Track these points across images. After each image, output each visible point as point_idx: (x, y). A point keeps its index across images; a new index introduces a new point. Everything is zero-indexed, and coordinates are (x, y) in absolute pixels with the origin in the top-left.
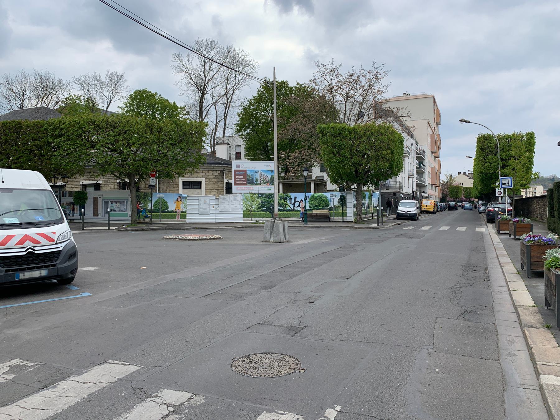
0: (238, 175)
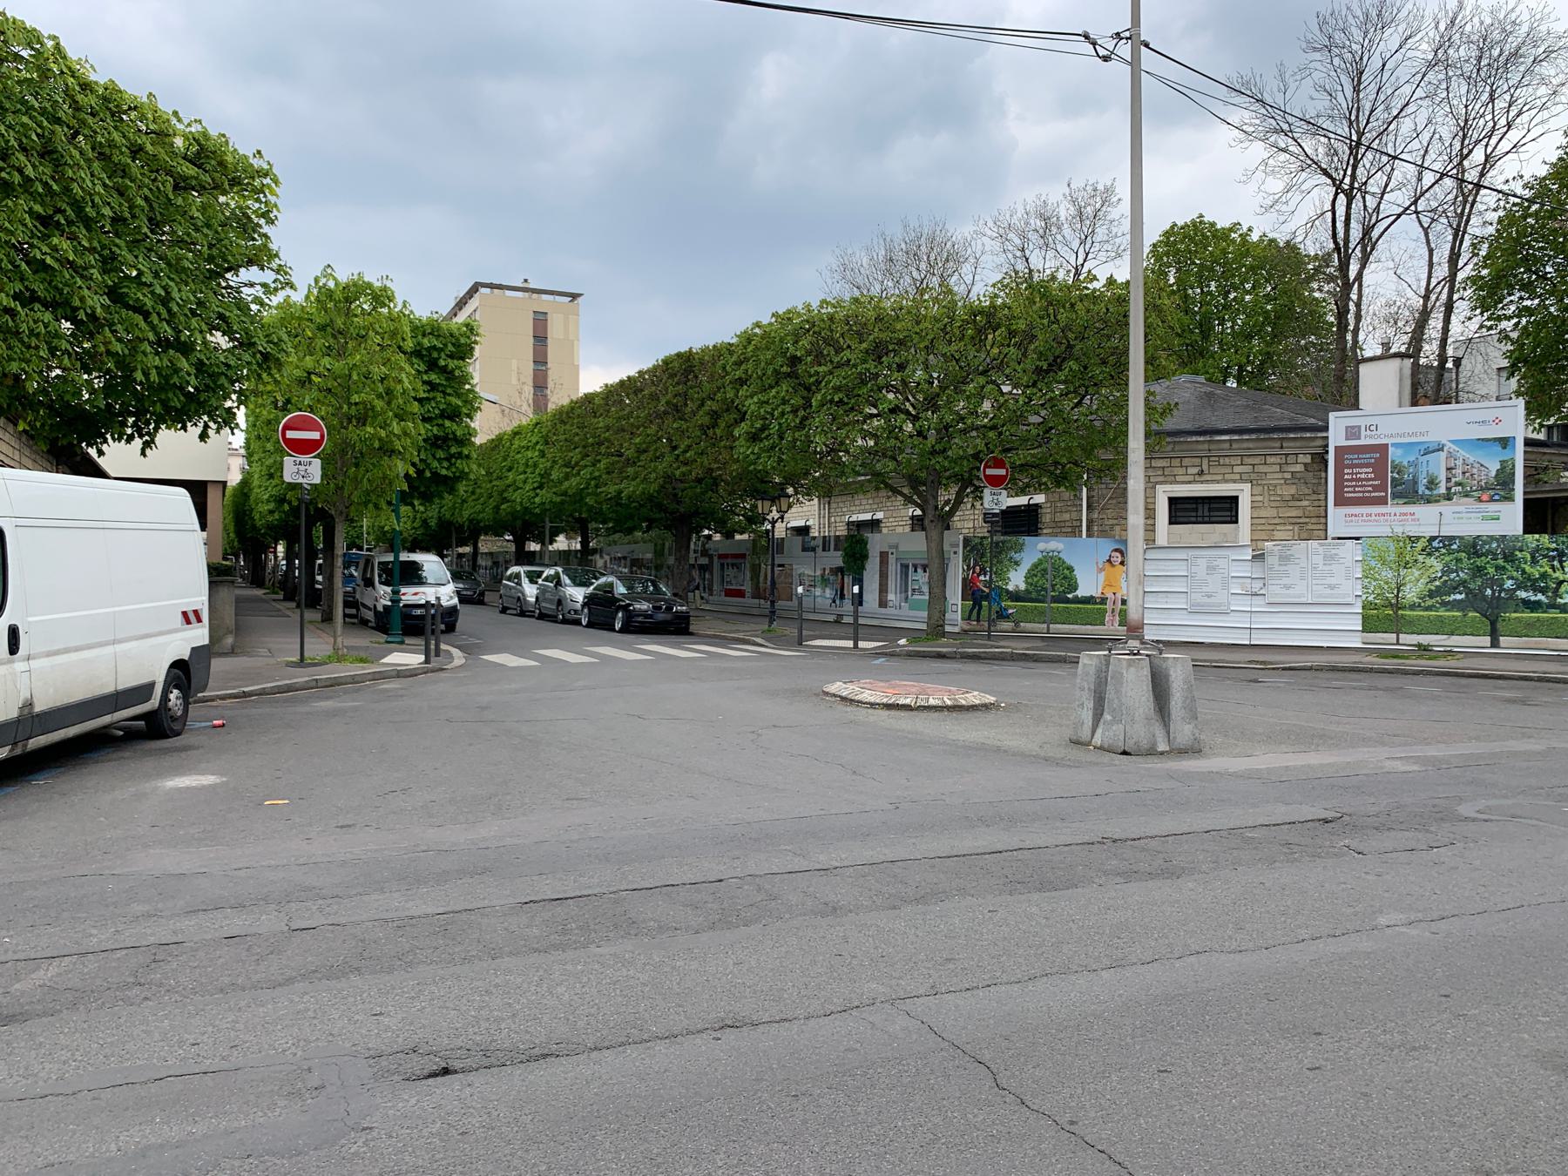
0: (1352, 466)
